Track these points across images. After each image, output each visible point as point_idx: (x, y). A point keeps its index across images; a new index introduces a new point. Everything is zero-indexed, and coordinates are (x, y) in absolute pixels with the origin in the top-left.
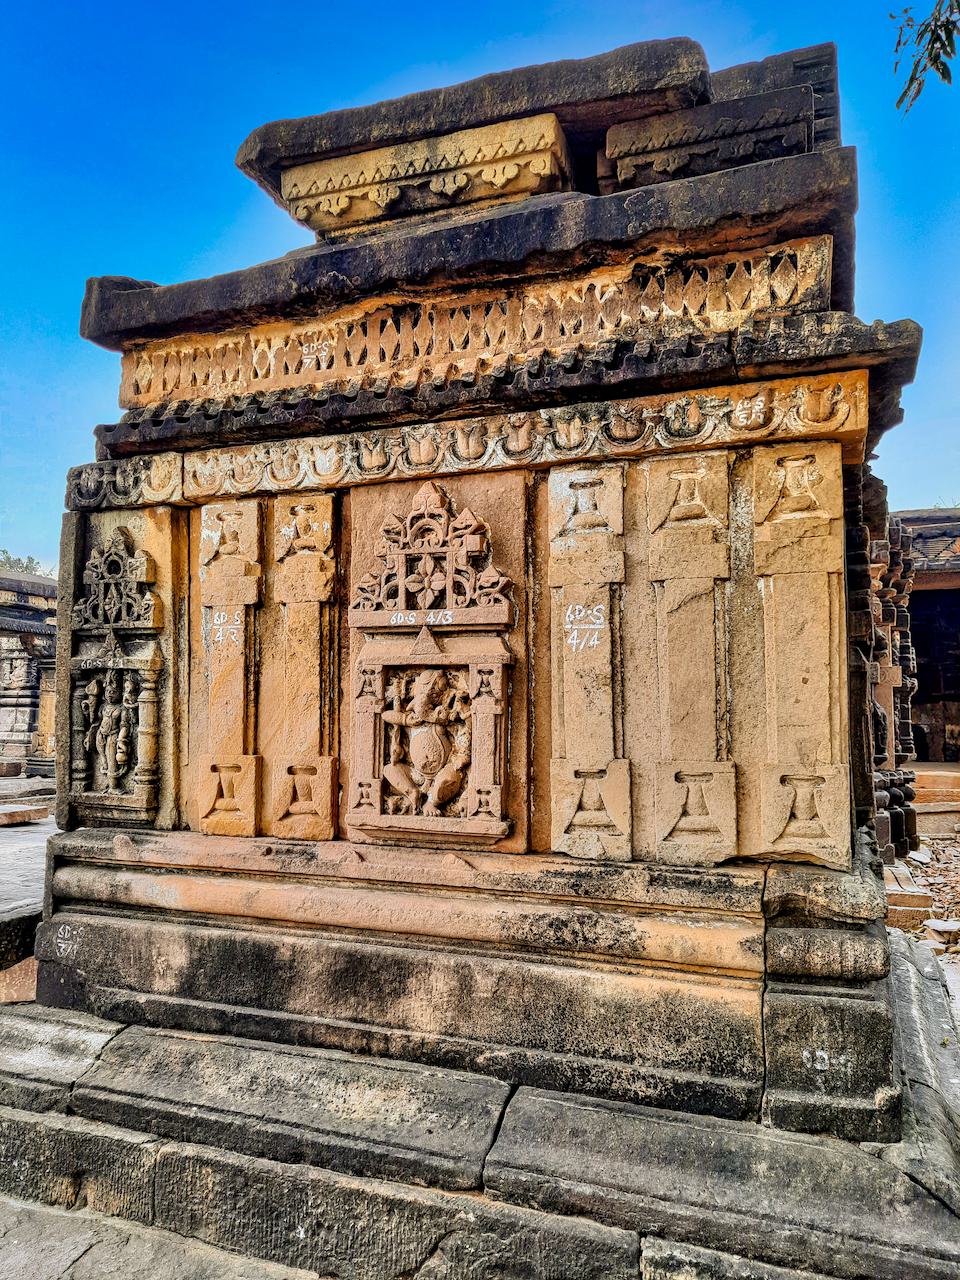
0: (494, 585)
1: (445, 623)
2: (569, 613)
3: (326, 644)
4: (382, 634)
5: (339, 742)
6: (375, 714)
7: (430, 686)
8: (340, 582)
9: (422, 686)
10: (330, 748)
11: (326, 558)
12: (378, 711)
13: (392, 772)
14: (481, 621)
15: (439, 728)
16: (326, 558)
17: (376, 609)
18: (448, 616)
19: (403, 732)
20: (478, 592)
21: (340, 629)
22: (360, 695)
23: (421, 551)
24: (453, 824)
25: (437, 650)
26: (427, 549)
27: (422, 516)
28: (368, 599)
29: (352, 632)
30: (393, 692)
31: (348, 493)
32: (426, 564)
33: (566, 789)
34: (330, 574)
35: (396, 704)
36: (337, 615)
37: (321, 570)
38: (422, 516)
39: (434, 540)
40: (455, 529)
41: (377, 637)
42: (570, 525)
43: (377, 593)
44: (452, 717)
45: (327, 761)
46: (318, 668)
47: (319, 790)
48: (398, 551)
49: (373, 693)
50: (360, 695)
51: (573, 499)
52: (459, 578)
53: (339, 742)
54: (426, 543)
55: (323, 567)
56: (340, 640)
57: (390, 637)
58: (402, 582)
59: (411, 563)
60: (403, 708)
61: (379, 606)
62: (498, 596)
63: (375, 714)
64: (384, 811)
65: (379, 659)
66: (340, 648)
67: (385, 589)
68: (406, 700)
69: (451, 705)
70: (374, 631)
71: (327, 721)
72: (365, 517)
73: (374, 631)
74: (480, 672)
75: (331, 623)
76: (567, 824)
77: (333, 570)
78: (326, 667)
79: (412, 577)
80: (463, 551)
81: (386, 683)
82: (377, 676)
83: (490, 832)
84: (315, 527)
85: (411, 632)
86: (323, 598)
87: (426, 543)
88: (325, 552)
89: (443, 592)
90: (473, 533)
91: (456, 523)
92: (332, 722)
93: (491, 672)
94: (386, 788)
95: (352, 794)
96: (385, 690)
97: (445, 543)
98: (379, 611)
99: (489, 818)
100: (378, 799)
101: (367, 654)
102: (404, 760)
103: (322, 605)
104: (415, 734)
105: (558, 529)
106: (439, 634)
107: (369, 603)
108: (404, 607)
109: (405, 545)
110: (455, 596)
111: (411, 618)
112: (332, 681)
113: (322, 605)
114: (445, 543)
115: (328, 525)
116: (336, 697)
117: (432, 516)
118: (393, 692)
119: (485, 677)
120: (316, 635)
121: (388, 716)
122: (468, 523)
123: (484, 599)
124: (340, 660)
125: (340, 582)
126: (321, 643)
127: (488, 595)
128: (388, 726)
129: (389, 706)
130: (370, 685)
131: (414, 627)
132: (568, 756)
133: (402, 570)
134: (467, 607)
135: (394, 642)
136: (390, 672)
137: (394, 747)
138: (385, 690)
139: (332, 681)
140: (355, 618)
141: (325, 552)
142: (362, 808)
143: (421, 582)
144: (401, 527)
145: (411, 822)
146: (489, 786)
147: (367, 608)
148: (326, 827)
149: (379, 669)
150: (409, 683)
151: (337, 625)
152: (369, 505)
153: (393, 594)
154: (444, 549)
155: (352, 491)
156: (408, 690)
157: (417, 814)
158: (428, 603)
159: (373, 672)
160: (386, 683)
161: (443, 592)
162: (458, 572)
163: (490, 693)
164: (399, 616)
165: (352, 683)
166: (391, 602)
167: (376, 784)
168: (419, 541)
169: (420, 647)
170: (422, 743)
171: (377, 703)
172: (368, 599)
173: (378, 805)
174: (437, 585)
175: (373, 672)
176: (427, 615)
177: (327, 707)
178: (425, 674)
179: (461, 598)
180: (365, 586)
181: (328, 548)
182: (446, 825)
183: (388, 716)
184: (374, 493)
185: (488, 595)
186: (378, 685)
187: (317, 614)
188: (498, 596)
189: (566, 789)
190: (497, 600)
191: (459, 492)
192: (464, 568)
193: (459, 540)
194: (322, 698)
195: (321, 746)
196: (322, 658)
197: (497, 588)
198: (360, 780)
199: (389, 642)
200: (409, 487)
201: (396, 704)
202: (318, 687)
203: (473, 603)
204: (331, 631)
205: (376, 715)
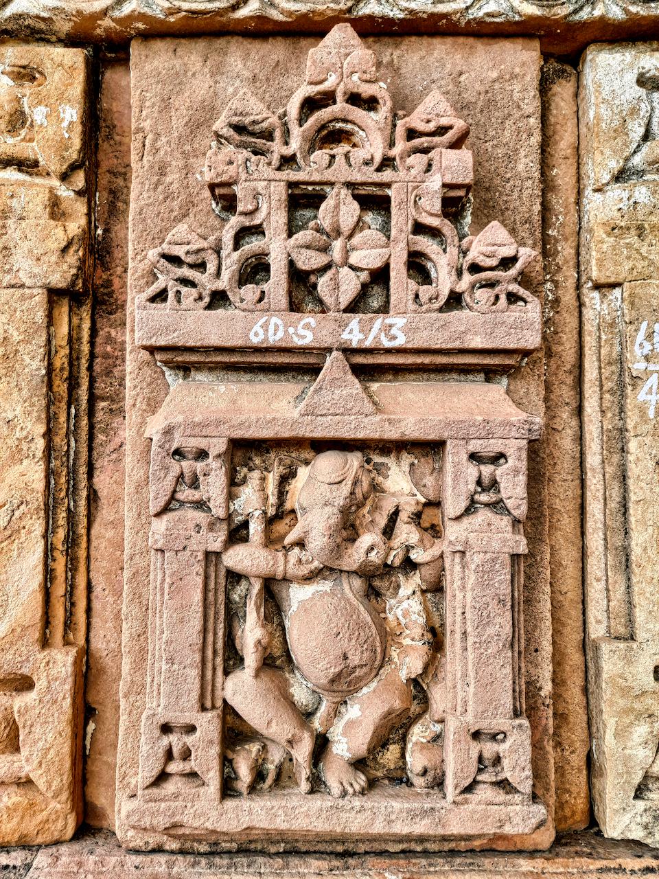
0: (507, 263)
1: (387, 344)
2: (641, 336)
3: (61, 387)
4: (211, 369)
5: (89, 610)
6: (207, 554)
7: (346, 489)
8: (98, 251)
9: (319, 487)
10: (69, 625)
11: (65, 192)
12: (216, 546)
13: (243, 690)
14: (477, 342)
15: (357, 583)
16: (65, 192)
17: (209, 307)
18: (395, 329)
19: (272, 591)
20: (467, 278)
21: (92, 356)
22: (166, 509)
23: (328, 175)
24: (413, 815)
25: (369, 407)
26: (340, 172)
27: (327, 98)
28: (186, 282)
29: (131, 363)
30: (250, 500)
31: (123, 61)
32: (340, 209)
33: (637, 705)
34: (76, 226)
35: (256, 528)
36: (86, 325)
37: (53, 216)
38: (327, 98)
39: (359, 155)
40: (412, 134)
41: (201, 377)
42: (637, 161)
43: (211, 267)
44: (395, 558)
45: (63, 661)
46: (40, 444)
47: (37, 730)
48: (269, 172)
49: (201, 505)
50: (166, 509)
51: (645, 107)
52: (426, 244)
53: (89, 610)
54: (340, 160)
55: (56, 210)
56: (92, 381)
57: (232, 376)
58: (277, 247)
59: (303, 200)
60: (271, 541)
61: (219, 299)
62: (514, 287)
63: (207, 554)
64: (228, 789)
65: (218, 423)
66: (92, 399)
67: (232, 261)
68: (280, 515)
69: (388, 531)
70: (183, 359)
71: (60, 565)
72: (166, 104)
73: (183, 359)
74: (473, 457)
75: (72, 340)
76: (637, 778)
77: (83, 221)
78: (59, 440)
79: (302, 237)
80: (434, 183)
81: (234, 483)
82: (213, 463)
83: (508, 829)
84: (38, 115)
85: (300, 366)
86: (60, 277)
87: (340, 160)
88: (64, 177)
89: (381, 276)
90: (456, 145)
91: (416, 120)
92: (72, 567)
93: (497, 458)
94: (235, 732)
95: (131, 753)
96: (231, 497)
97: (387, 162)
98: (220, 312)
99: (501, 796)
100: (215, 764)
101: (160, 416)
102: (277, 661)
103: (54, 295)
104: (297, 596)
105: (615, 165)
106: (369, 368)
107: (194, 292)
108: (284, 302)
109: (288, 161)
110: (412, 285)
111: (305, 331)
112: (73, 473)
113: (54, 295)
114: (387, 162)
115: (72, 113)
116: (82, 509)
117: (354, 99)
118: (250, 500)
119: (487, 470)
120: (34, 365)
121: (237, 558)
122: (444, 121)
123: (483, 295)
124: (91, 427)
125: (98, 251)
126: (50, 385)
127: (491, 284)
128: (234, 577)
129: (238, 534)
130: (194, 484)
131: (304, 351)
132: (641, 635)
133: (280, 218)
134: (441, 310)
135: (248, 388)
136: (244, 451)
137: (251, 633)
138: (231, 497)
139: (73, 473)
140: (142, 322)
141: (64, 177)
142: (170, 787)
143: (325, 249)
144: (274, 120)
145: (294, 812)
146: (502, 722)
147: (188, 302)
148: (57, 812)
149: (218, 446)
150: (285, 480)
151: (85, 348)
152: (178, 80)
153: (255, 270)
154: (387, 175)
155: (135, 49)
156: (282, 495)
157: (312, 791)
158: (345, 299)
159: (202, 455)
160: (234, 483)
161: (381, 276)
162: (419, 228)
163: (497, 506)
164: (269, 325)
165: (128, 482)
166: (250, 292)
167: (209, 726)
168: (321, 156)
169: (325, 398)
170: (317, 619)
171: (211, 527)
172: (186, 282)
173: (213, 779)
174: (367, 257)
175: (202, 455)
176: (343, 325)
177: (61, 534)
178: (327, 463)
179: (426, 291)
180: (180, 251)
181: (73, 168)
182: (389, 815)
183: (237, 558)
184: (192, 56)
185: (491, 284)
186: (214, 486)
187: (40, 316)
188: (514, 287)
189: (637, 705)
190: (513, 298)
191: (397, 71)
192: (434, 222)
193: (424, 158)
194: (49, 510)
195: (47, 621)
196: (50, 419)
197: (513, 272)
198: (164, 716)
199: (234, 387)
200: (276, 50)
201: (256, 528)
202: (40, 486)
203: (455, 300)
204: (73, 360)
205: (211, 558)
